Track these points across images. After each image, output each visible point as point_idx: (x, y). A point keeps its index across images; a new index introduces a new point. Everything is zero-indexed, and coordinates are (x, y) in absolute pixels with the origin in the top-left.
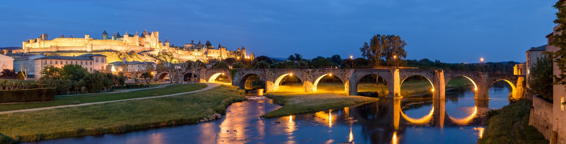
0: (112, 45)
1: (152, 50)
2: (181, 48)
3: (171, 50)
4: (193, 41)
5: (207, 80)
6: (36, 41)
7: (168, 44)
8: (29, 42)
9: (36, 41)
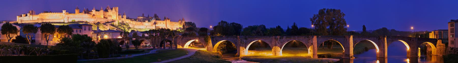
0: (83, 18)
1: (113, 21)
2: (135, 20)
3: (128, 21)
4: (143, 14)
5: (183, 46)
6: (26, 15)
7: (125, 17)
8: (21, 16)
9: (26, 15)
